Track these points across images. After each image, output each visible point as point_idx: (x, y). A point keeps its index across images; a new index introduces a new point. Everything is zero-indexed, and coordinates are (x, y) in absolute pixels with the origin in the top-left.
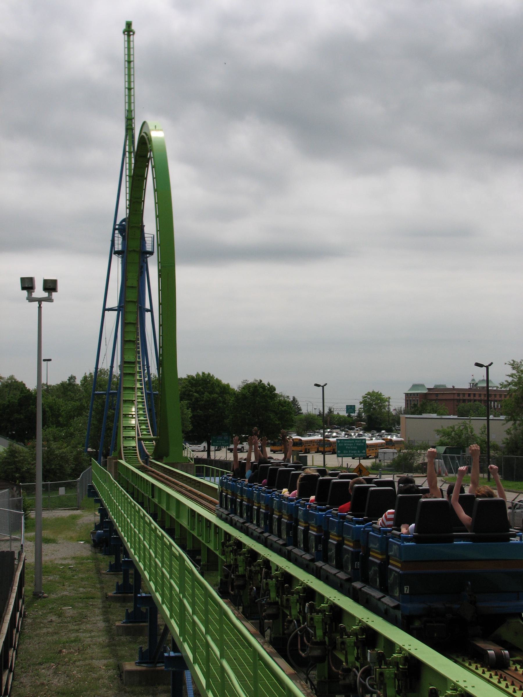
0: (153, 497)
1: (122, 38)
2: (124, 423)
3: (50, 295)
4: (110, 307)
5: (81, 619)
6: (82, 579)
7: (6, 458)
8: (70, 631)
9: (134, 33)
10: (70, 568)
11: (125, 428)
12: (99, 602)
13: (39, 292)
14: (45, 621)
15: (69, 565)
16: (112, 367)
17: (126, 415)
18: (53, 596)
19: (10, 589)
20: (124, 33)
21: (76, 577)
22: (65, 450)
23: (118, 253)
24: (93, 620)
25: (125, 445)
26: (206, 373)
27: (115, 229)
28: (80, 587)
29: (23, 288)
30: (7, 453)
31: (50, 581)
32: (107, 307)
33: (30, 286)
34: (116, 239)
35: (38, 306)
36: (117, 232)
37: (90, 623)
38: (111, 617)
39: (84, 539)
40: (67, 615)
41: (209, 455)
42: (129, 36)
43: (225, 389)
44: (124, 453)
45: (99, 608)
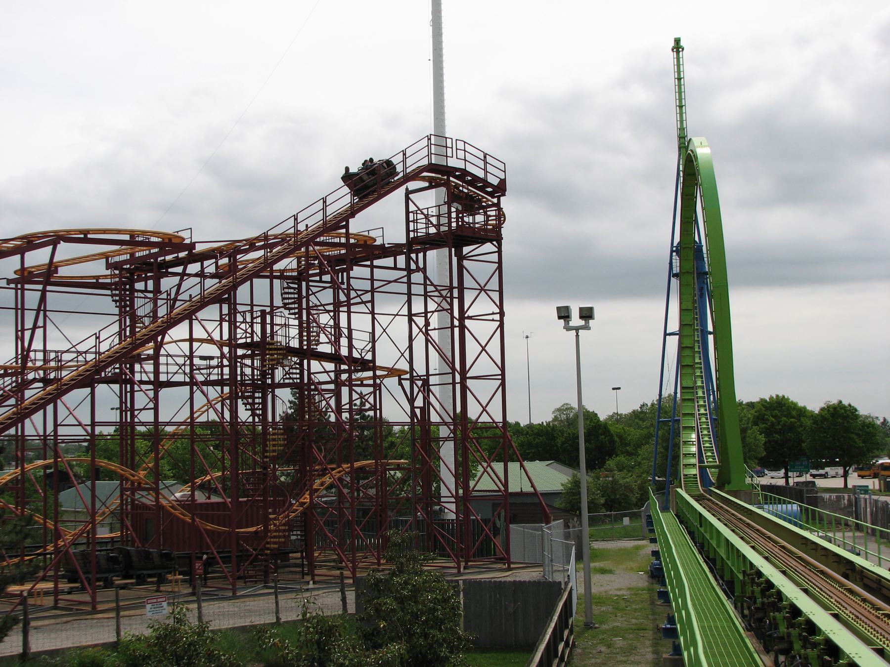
0: (701, 526)
1: (671, 55)
2: (684, 450)
3: (587, 323)
4: (671, 332)
5: (630, 650)
6: (635, 610)
7: (570, 489)
8: (618, 662)
9: (683, 49)
10: (624, 599)
11: (685, 455)
12: (649, 634)
13: (576, 320)
14: (594, 652)
15: (623, 595)
16: (676, 393)
17: (685, 442)
18: (604, 627)
19: (550, 618)
20: (673, 50)
21: (629, 608)
22: (628, 480)
23: (676, 275)
24: (642, 652)
25: (686, 473)
26: (780, 395)
27: (672, 251)
28: (632, 618)
29: (560, 318)
30: (571, 483)
31: (603, 612)
32: (668, 332)
33: (566, 315)
34: (674, 261)
35: (575, 334)
36: (674, 254)
37: (639, 654)
38: (661, 649)
39: (644, 569)
40: (616, 646)
41: (787, 482)
42: (678, 52)
43: (802, 412)
44: (684, 481)
45: (649, 640)
